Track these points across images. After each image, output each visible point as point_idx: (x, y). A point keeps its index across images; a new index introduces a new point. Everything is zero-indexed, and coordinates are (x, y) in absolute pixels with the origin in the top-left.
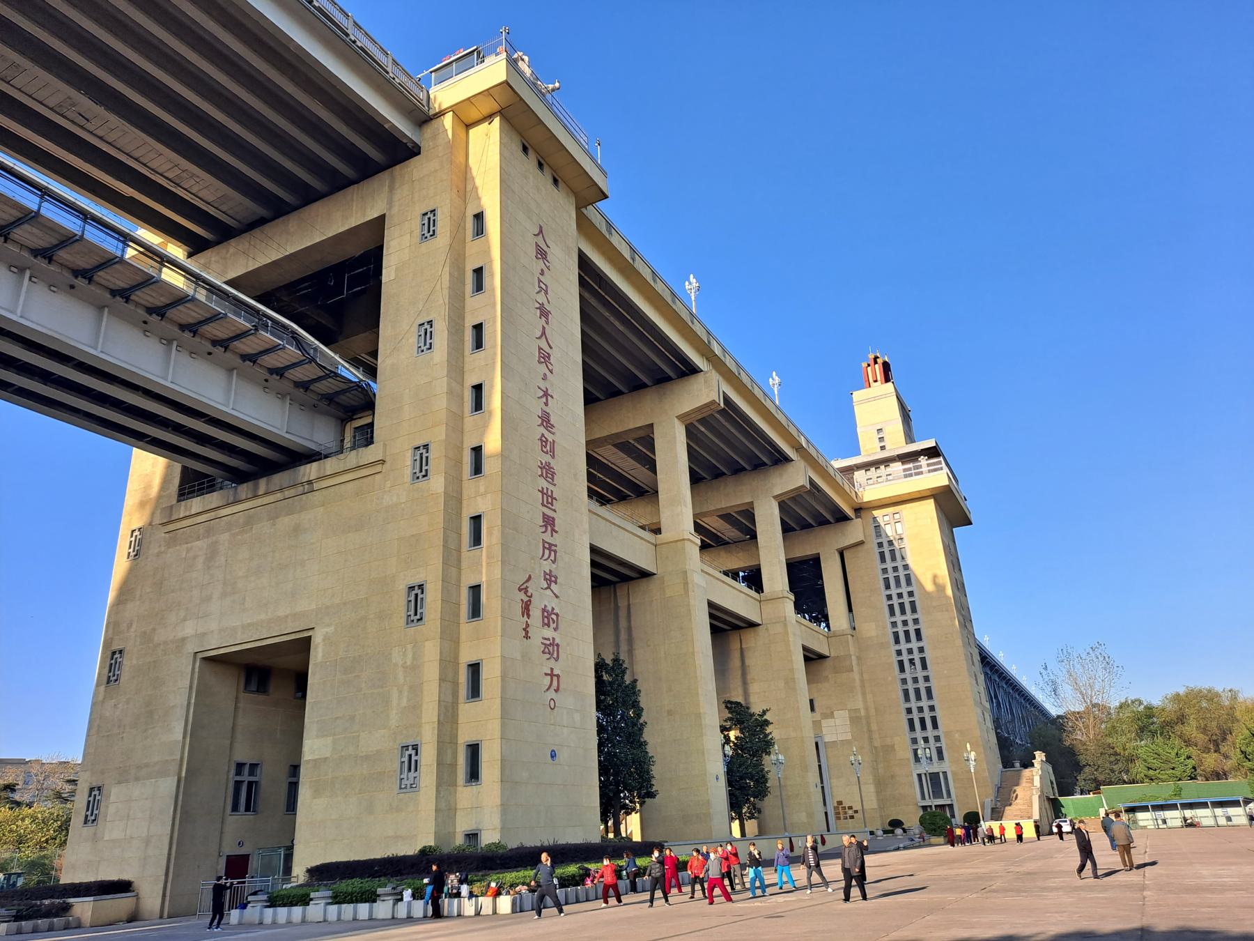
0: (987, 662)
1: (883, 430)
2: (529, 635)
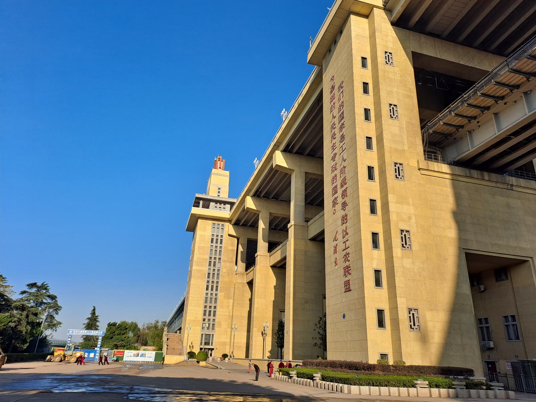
0: (323, 88)
1: (221, 189)
2: (39, 284)
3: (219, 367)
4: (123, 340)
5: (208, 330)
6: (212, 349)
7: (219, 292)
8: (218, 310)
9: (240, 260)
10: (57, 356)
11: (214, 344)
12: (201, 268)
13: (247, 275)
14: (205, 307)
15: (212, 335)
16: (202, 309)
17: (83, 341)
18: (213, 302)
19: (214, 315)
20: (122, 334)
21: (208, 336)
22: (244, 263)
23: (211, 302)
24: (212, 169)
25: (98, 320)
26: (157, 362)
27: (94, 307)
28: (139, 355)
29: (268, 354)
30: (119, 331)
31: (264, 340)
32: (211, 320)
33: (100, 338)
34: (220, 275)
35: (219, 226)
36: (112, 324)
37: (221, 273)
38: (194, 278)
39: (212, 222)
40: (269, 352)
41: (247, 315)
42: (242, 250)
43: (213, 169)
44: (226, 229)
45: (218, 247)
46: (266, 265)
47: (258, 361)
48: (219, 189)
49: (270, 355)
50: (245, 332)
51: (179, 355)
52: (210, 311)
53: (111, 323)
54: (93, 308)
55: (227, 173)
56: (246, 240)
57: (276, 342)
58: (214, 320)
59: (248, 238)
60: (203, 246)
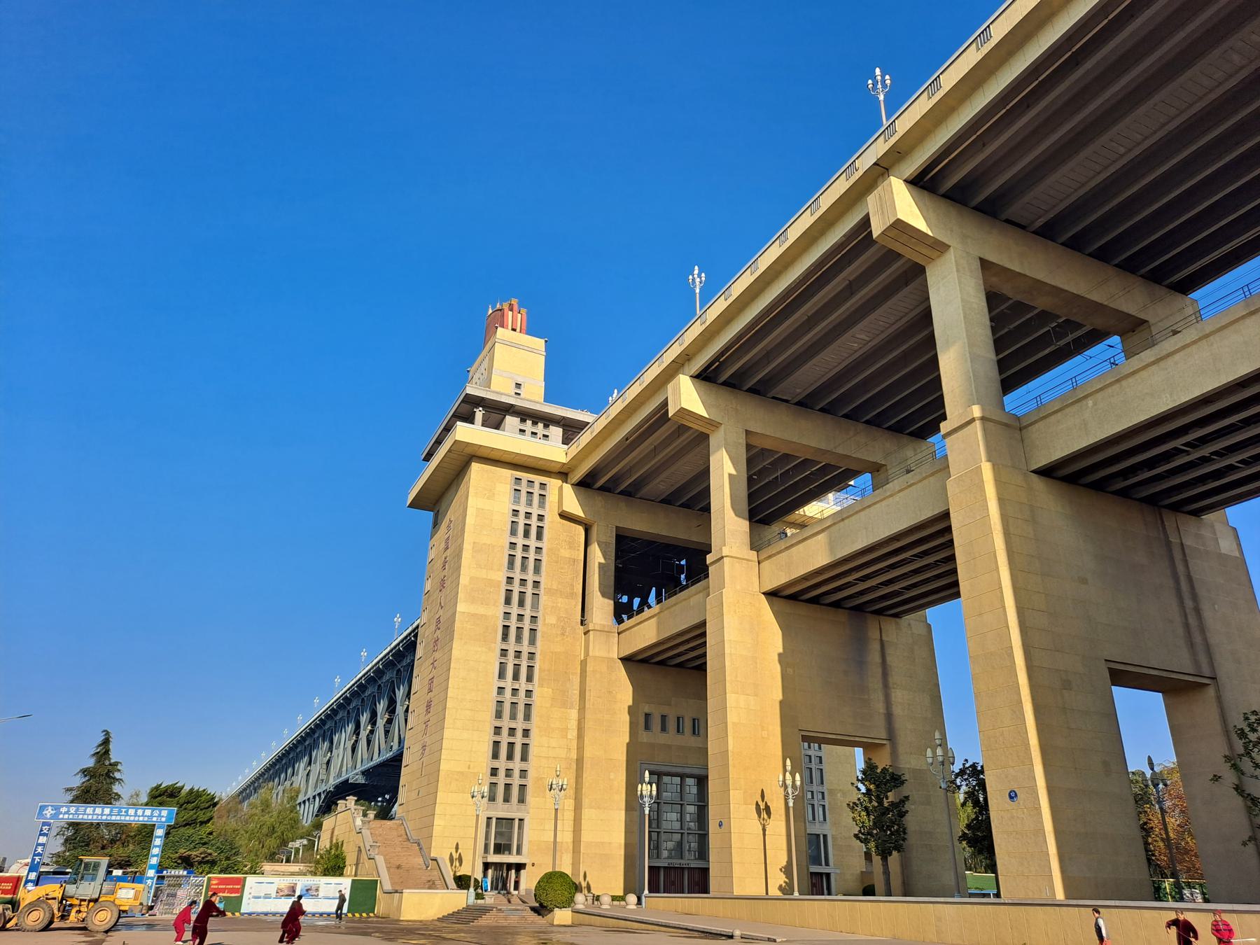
1: (522, 386)
3: (737, 933)
4: (204, 844)
5: (507, 805)
6: (519, 867)
7: (535, 686)
8: (535, 741)
9: (597, 589)
10: (33, 906)
11: (525, 849)
12: (481, 610)
13: (620, 636)
14: (498, 730)
15: (520, 820)
16: (487, 738)
17: (63, 849)
18: (520, 715)
19: (524, 758)
20: (202, 823)
21: (505, 824)
22: (609, 598)
23: (513, 717)
24: (497, 328)
25: (117, 775)
26: (357, 915)
27: (107, 733)
28: (294, 891)
29: (777, 879)
30: (192, 813)
31: (764, 830)
32: (516, 773)
33: (160, 832)
34: (539, 634)
35: (532, 487)
36: (166, 791)
37: (540, 627)
38: (461, 639)
39: (512, 474)
40: (781, 870)
41: (625, 758)
42: (602, 561)
43: (500, 329)
44: (552, 497)
45: (532, 550)
46: (751, 589)
47: (736, 900)
48: (518, 385)
49: (785, 882)
50: (621, 810)
51: (430, 888)
52: (511, 745)
53: (163, 786)
54: (101, 738)
55: (540, 343)
56: (612, 532)
57: (856, 836)
58: (523, 773)
59: (616, 527)
60: (489, 542)
